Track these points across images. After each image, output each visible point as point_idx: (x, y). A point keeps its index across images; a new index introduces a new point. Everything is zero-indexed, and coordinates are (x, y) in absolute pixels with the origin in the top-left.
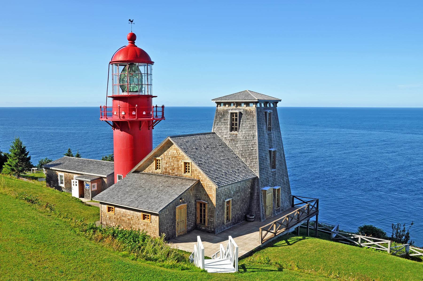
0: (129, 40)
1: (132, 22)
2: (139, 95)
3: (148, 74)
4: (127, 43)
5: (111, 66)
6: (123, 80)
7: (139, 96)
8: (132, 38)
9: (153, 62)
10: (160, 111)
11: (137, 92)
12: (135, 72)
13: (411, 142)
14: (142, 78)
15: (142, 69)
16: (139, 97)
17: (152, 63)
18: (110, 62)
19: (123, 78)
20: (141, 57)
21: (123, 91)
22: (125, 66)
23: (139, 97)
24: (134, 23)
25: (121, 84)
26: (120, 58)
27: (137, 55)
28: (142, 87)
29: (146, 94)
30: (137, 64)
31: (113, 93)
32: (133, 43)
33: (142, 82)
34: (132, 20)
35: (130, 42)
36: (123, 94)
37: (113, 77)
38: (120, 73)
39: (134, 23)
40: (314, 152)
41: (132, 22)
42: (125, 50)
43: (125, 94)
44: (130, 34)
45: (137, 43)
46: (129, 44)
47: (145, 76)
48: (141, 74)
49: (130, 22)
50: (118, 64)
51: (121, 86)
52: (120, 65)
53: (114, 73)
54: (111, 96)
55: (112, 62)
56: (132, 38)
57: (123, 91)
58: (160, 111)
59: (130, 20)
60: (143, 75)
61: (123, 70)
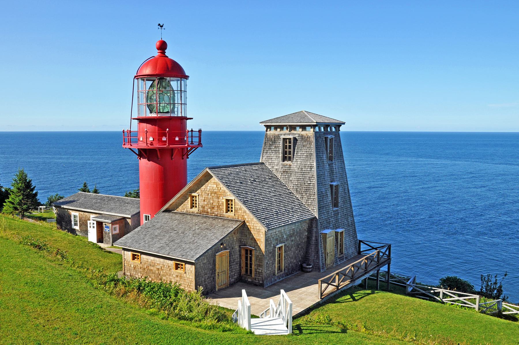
0: (158, 49)
1: (162, 27)
2: (170, 117)
3: (181, 91)
4: (156, 53)
5: (136, 80)
6: (151, 98)
7: (171, 118)
8: (163, 46)
9: (188, 77)
11: (168, 112)
12: (165, 88)
14: (174, 96)
15: (174, 84)
16: (171, 119)
17: (186, 77)
18: (135, 77)
19: (151, 96)
21: (151, 112)
22: (154, 81)
23: (171, 119)
24: (164, 29)
25: (149, 103)
26: (148, 71)
27: (168, 68)
28: (174, 107)
29: (180, 115)
30: (168, 79)
31: (139, 114)
32: (163, 53)
33: (174, 100)
34: (161, 25)
35: (160, 51)
36: (150, 116)
37: (138, 94)
38: (147, 89)
39: (164, 29)
41: (162, 27)
42: (153, 62)
43: (154, 115)
45: (168, 53)
46: (158, 54)
47: (178, 93)
48: (173, 91)
49: (159, 27)
50: (145, 79)
51: (149, 106)
52: (147, 80)
54: (136, 117)
55: (138, 76)
56: (163, 46)
57: (151, 112)
59: (159, 25)
60: (176, 92)
61: (151, 86)
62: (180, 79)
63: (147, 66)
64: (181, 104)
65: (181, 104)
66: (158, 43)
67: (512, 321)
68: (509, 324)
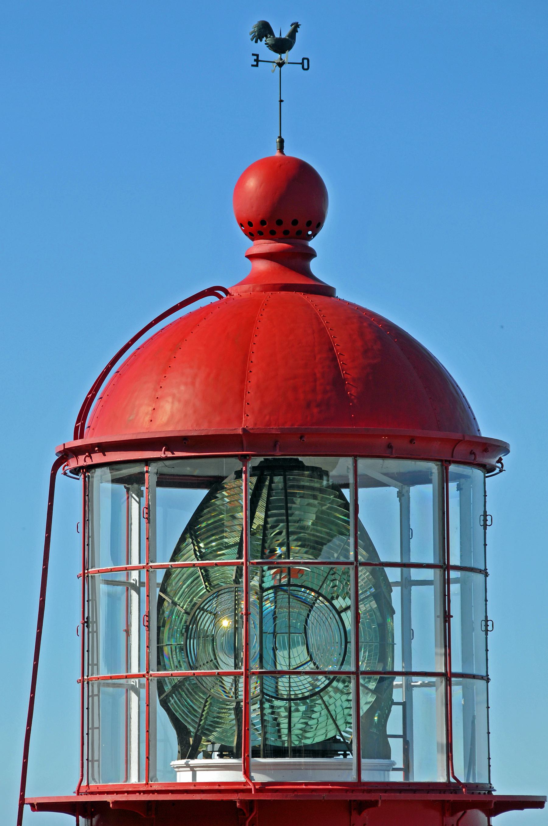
0: (254, 229)
1: (282, 46)
2: (358, 786)
3: (444, 566)
4: (235, 262)
5: (70, 487)
7: (361, 799)
8: (288, 208)
9: (497, 447)
10: (355, 462)
11: (327, 749)
12: (315, 546)
13: (263, 770)
15: (389, 509)
16: (361, 806)
17: (484, 454)
18: (66, 455)
19: (194, 612)
20: (384, 401)
21: (189, 750)
22: (214, 484)
23: (361, 806)
24: (305, 64)
25: (176, 671)
26: (166, 409)
27: (338, 382)
28: (383, 705)
29: (429, 770)
30: (341, 467)
31: (86, 761)
32: (296, 258)
33: (384, 648)
34: (281, 31)
35: (264, 246)
37: (87, 599)
38: (163, 559)
39: (305, 64)
40: (225, 713)
41: (282, 46)
42: (210, 333)
43: (214, 772)
44: (267, 164)
46: (250, 268)
47: (407, 584)
48: (378, 566)
49: (262, 47)
50: (151, 473)
51: (168, 694)
52: (164, 481)
53: (104, 560)
54: (67, 792)
55: (89, 450)
56: (288, 208)
57: (189, 750)
58: (355, 462)
59: (264, 30)
61: (191, 530)
62: (433, 467)
63: (165, 370)
64: (448, 676)
65: (448, 676)
66: (252, 183)
67: (371, 801)
68: (120, 673)
